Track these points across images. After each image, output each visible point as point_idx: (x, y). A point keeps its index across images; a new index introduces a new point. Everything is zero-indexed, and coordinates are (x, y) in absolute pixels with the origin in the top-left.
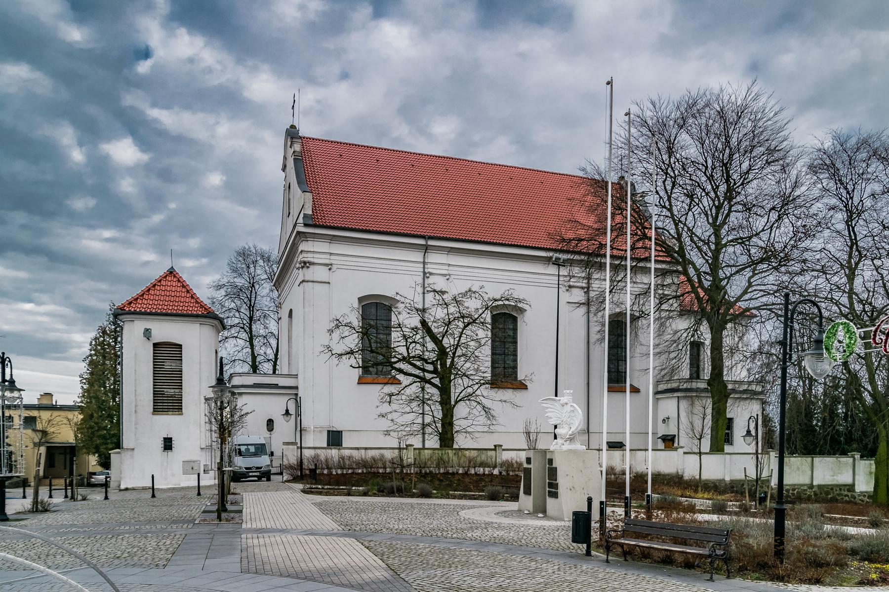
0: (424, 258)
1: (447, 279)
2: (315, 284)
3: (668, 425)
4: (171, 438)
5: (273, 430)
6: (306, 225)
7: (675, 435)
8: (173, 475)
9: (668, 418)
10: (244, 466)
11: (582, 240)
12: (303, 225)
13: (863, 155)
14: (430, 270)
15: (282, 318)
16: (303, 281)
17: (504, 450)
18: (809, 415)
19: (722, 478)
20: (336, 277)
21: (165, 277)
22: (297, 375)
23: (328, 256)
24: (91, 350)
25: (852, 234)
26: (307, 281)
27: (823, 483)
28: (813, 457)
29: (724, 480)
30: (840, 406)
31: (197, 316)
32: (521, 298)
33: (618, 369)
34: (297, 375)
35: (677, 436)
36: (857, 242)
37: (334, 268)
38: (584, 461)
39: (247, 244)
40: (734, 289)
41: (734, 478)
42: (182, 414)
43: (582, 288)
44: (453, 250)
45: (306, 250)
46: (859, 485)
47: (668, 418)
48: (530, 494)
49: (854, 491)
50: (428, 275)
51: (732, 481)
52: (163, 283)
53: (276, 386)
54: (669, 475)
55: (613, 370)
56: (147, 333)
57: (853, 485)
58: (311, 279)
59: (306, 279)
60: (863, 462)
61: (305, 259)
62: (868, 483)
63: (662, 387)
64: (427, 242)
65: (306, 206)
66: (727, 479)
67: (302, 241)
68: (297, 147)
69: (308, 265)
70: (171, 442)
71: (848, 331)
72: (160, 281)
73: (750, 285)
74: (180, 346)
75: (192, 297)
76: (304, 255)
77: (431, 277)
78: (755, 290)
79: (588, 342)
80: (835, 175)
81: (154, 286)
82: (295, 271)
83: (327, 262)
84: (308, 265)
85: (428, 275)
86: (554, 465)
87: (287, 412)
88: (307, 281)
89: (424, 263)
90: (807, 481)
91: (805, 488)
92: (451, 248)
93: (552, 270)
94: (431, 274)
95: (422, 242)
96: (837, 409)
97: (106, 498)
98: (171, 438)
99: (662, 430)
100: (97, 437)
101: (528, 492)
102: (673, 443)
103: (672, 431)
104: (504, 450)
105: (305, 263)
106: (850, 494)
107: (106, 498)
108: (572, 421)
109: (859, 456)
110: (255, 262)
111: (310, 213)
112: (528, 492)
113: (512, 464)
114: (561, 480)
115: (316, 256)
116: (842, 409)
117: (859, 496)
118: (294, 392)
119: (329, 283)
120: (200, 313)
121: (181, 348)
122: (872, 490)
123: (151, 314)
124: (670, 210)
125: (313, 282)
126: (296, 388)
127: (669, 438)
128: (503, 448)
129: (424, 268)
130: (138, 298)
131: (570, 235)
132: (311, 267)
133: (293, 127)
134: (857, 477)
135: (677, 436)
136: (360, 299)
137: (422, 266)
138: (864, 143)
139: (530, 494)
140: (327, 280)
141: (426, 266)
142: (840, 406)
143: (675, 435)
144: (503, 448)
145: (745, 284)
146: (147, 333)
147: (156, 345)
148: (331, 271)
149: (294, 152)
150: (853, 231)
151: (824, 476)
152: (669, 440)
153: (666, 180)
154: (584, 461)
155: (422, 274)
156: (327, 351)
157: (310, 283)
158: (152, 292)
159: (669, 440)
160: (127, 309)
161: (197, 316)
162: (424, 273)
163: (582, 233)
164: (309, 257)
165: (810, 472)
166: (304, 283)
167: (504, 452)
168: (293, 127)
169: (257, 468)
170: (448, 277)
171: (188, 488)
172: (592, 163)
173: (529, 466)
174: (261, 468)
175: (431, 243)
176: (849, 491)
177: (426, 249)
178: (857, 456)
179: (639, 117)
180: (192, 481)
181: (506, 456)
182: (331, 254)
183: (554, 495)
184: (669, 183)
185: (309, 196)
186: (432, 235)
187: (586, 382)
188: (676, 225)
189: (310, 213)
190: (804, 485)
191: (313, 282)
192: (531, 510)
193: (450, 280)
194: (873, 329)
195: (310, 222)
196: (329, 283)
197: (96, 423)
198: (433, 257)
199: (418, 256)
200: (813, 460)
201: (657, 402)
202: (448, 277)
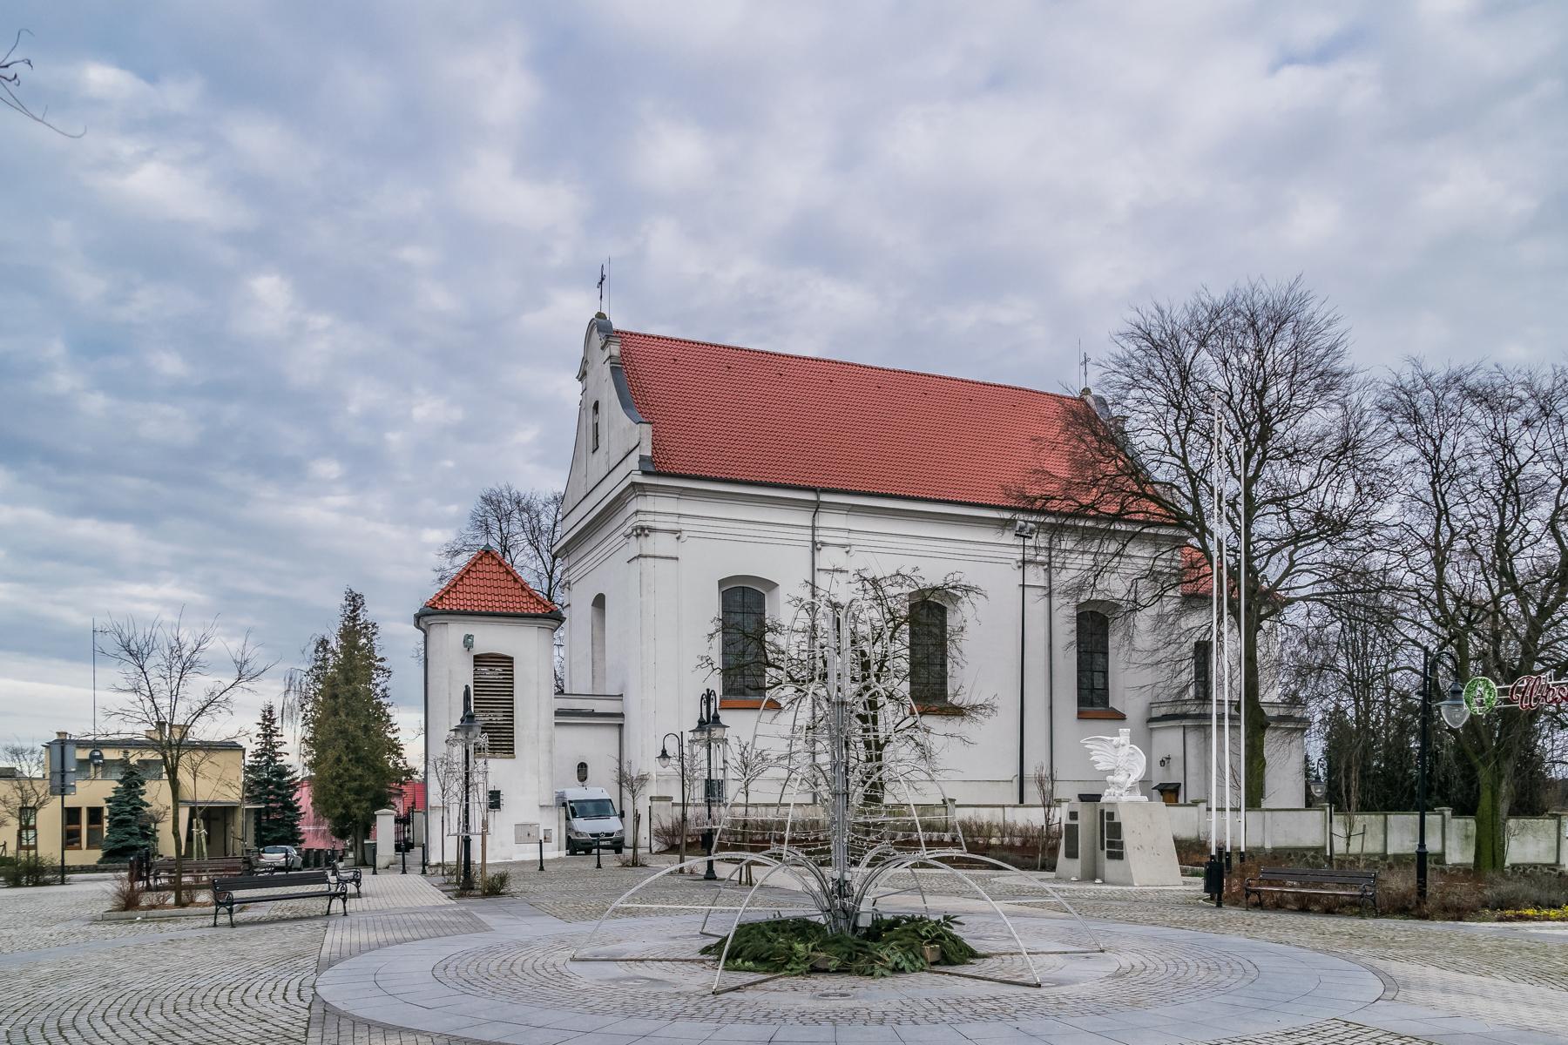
0: (814, 520)
1: (847, 552)
2: (657, 560)
3: (1168, 768)
4: (499, 792)
5: (586, 778)
6: (645, 473)
7: (1180, 784)
8: (502, 845)
9: (1169, 758)
10: (588, 831)
11: (1053, 498)
12: (640, 472)
13: (1452, 394)
14: (821, 539)
15: (572, 605)
16: (640, 556)
17: (957, 806)
18: (1367, 751)
19: (1260, 845)
20: (684, 550)
21: (481, 558)
22: (621, 695)
23: (675, 519)
24: (316, 660)
25: (1441, 502)
26: (646, 557)
27: (1401, 852)
28: (1386, 815)
29: (1263, 848)
30: (1413, 738)
31: (536, 616)
32: (973, 585)
33: (1093, 684)
34: (621, 695)
35: (1182, 785)
36: (1446, 510)
37: (684, 535)
38: (1151, 816)
39: (497, 484)
40: (1273, 571)
41: (1277, 845)
42: (514, 758)
43: (1042, 564)
44: (854, 509)
45: (643, 509)
46: (1450, 854)
47: (1169, 758)
48: (1077, 857)
49: (1444, 863)
50: (819, 546)
51: (1275, 850)
52: (479, 567)
53: (592, 714)
54: (1186, 841)
55: (1085, 686)
56: (468, 642)
57: (1443, 854)
58: (651, 553)
59: (644, 553)
60: (1455, 821)
61: (643, 524)
62: (1463, 852)
63: (1156, 713)
64: (818, 498)
65: (642, 445)
66: (1268, 846)
67: (637, 496)
68: (615, 350)
69: (646, 532)
70: (499, 797)
71: (1488, 687)
72: (474, 565)
73: (1292, 564)
74: (510, 660)
75: (523, 589)
76: (641, 517)
77: (823, 548)
78: (1299, 571)
79: (1050, 645)
80: (1415, 417)
81: (468, 572)
82: (618, 538)
83: (674, 527)
84: (646, 532)
85: (819, 546)
86: (1116, 820)
87: (664, 754)
88: (646, 557)
89: (813, 528)
90: (1378, 849)
91: (1376, 859)
92: (853, 505)
93: (1009, 537)
94: (823, 544)
95: (811, 497)
96: (1409, 743)
97: (599, 866)
98: (499, 792)
99: (1159, 777)
100: (348, 790)
101: (1072, 854)
102: (1177, 795)
103: (1175, 776)
104: (957, 806)
105: (643, 529)
106: (1438, 867)
107: (599, 866)
108: (1131, 767)
109: (1450, 813)
110: (508, 515)
111: (650, 454)
112: (1072, 854)
113: (970, 827)
114: (1127, 837)
115: (658, 518)
116: (1416, 741)
117: (1451, 869)
118: (618, 721)
119: (677, 559)
120: (540, 612)
121: (512, 662)
122: (1471, 860)
123: (472, 614)
124: (1184, 460)
125: (655, 557)
126: (621, 715)
127: (1172, 788)
128: (956, 803)
129: (813, 535)
130: (449, 591)
131: (1036, 491)
132: (652, 534)
133: (600, 315)
134: (1447, 843)
135: (1182, 785)
136: (721, 583)
137: (810, 532)
138: (1454, 380)
139: (1077, 857)
140: (674, 555)
141: (816, 533)
142: (1413, 738)
143: (1180, 784)
144: (956, 803)
145: (1286, 563)
146: (468, 642)
147: (475, 657)
148: (681, 540)
149: (610, 357)
150: (1443, 499)
151: (1402, 841)
152: (1171, 791)
153: (1178, 418)
154: (1151, 816)
155: (810, 544)
156: (706, 664)
157: (649, 559)
158: (466, 581)
159: (1171, 791)
160: (440, 607)
161: (536, 616)
162: (814, 543)
163: (1052, 488)
164: (648, 521)
165: (1383, 836)
166: (640, 559)
167: (958, 810)
168: (600, 315)
169: (607, 835)
170: (848, 549)
171: (523, 863)
172: (1070, 389)
173: (1075, 822)
174: (612, 834)
175: (825, 498)
176: (1437, 862)
177: (817, 507)
178: (1448, 813)
179: (1139, 328)
180: (530, 853)
181: (961, 815)
182: (680, 515)
183: (1117, 853)
184: (1183, 423)
185: (647, 428)
186: (825, 486)
187: (1048, 705)
188: (1193, 482)
189: (650, 454)
190: (1374, 855)
191: (655, 557)
192: (1080, 876)
193: (850, 554)
194: (1511, 686)
195: (651, 469)
196: (677, 559)
197: (346, 770)
198: (825, 520)
199: (804, 518)
200: (1386, 819)
201: (1151, 735)
202: (848, 549)
